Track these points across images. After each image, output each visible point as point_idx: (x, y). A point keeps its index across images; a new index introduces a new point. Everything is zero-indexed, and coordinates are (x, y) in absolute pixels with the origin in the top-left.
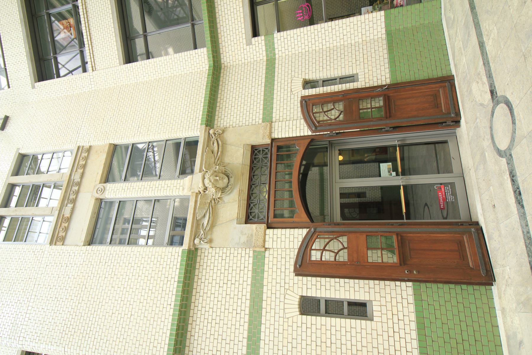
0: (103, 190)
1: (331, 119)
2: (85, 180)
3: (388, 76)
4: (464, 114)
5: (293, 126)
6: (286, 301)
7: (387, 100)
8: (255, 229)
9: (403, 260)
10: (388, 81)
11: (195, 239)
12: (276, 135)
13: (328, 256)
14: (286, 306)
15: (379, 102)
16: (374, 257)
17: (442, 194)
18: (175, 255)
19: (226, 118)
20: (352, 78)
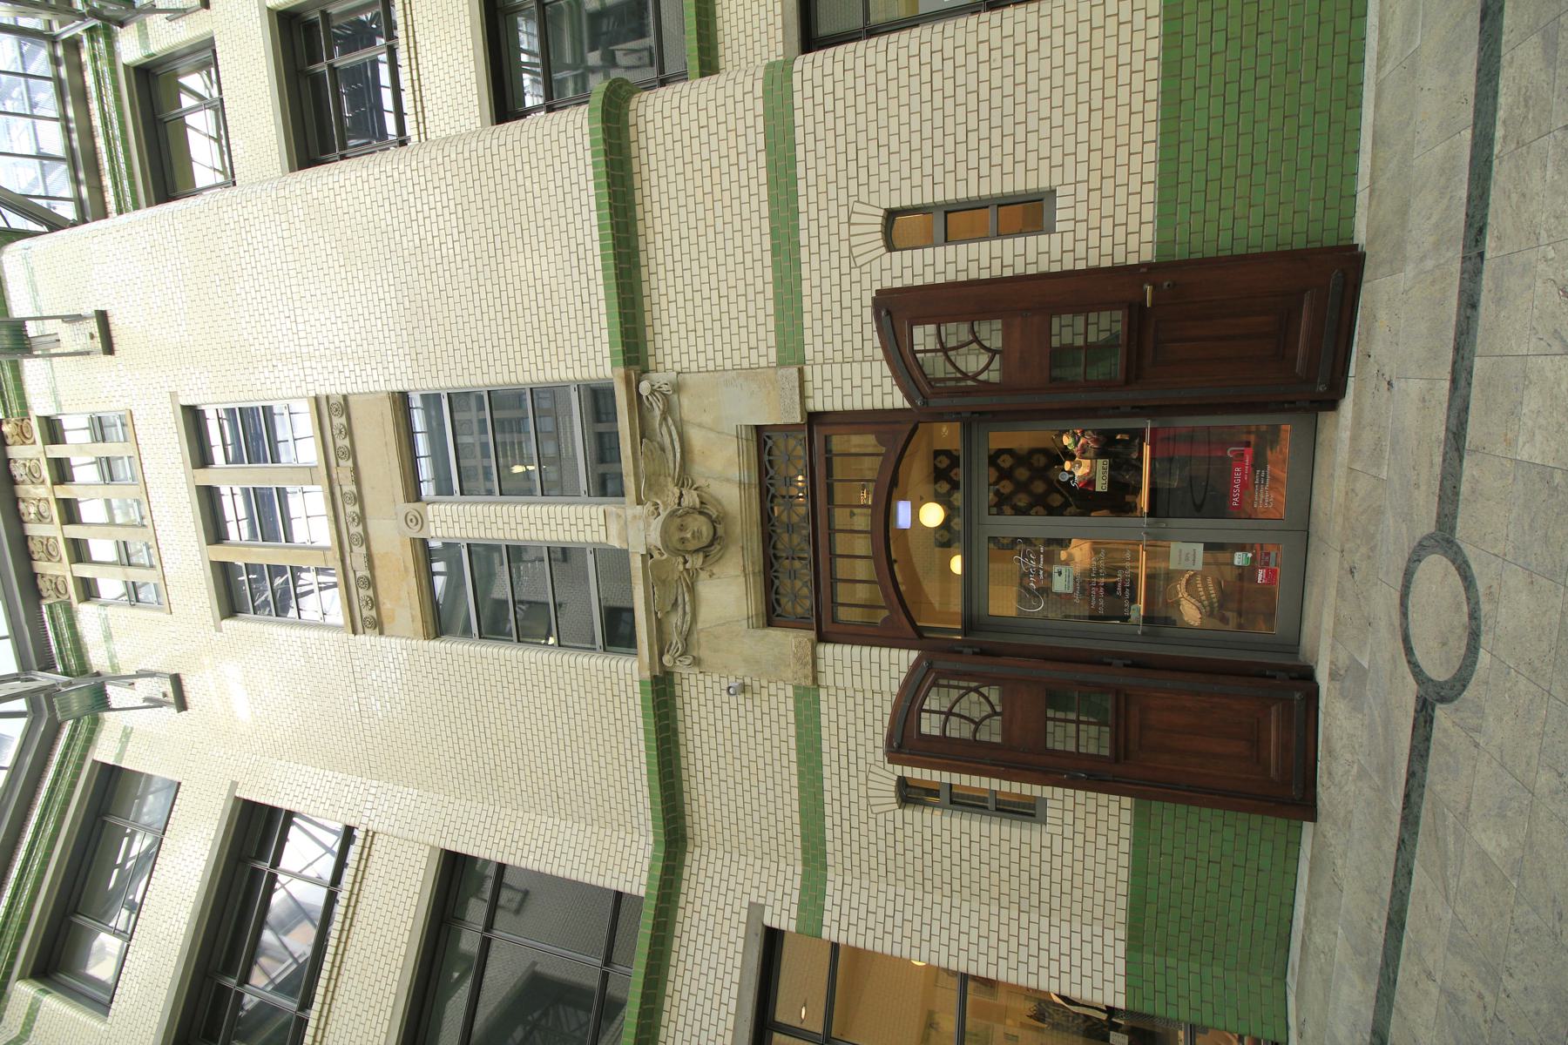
0: (420, 520)
1: (965, 376)
2: (378, 573)
3: (1148, 232)
4: (1357, 396)
5: (859, 380)
6: (871, 784)
7: (1137, 315)
8: (790, 641)
9: (1121, 749)
10: (1148, 254)
11: (661, 655)
12: (816, 404)
13: (958, 729)
14: (871, 793)
15: (1106, 325)
16: (1062, 736)
17: (1243, 472)
18: (627, 672)
19: (677, 346)
20: (1029, 212)
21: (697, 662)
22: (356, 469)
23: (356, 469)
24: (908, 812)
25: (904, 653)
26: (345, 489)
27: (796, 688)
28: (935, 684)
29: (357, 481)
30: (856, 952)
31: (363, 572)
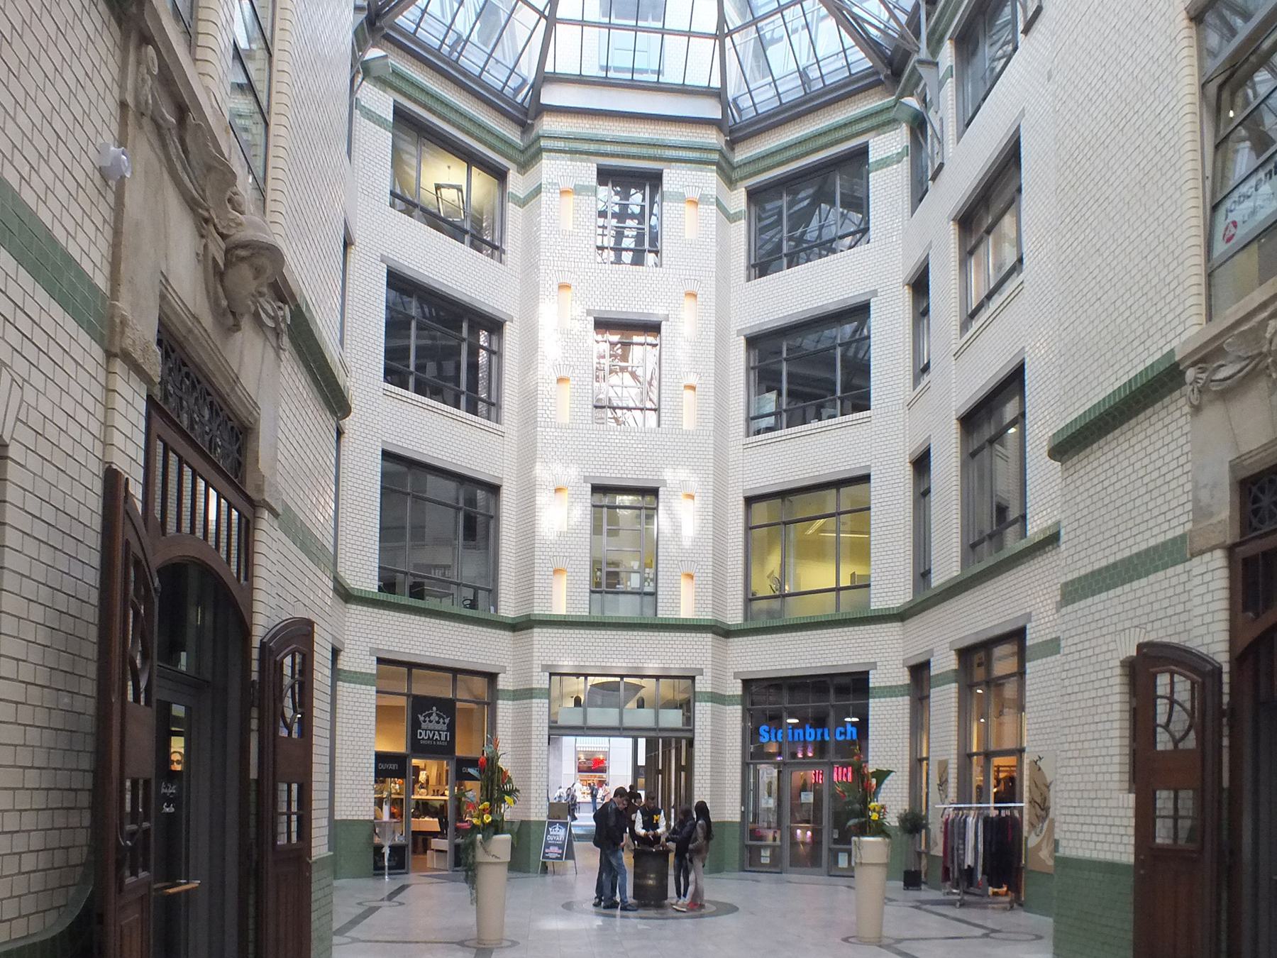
11: (1193, 364)
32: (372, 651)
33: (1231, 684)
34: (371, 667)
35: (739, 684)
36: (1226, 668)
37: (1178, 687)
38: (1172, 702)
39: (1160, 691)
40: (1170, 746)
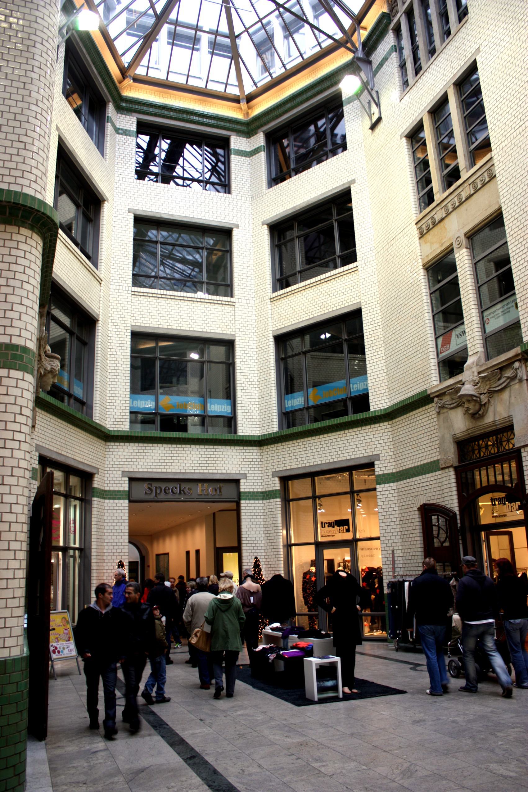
11: (437, 396)
18: (432, 381)
21: (439, 413)
22: (471, 196)
23: (471, 196)
24: (417, 512)
25: (456, 505)
26: (462, 193)
27: (438, 460)
28: (446, 520)
29: (467, 199)
30: (376, 497)
31: (464, 195)
32: (274, 475)
33: (461, 519)
34: (124, 485)
35: (277, 481)
36: (458, 513)
37: (436, 521)
38: (438, 526)
39: (12, 372)
40: (440, 545)
